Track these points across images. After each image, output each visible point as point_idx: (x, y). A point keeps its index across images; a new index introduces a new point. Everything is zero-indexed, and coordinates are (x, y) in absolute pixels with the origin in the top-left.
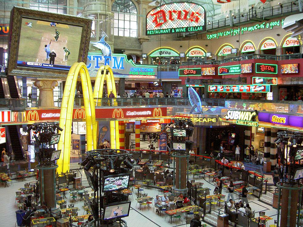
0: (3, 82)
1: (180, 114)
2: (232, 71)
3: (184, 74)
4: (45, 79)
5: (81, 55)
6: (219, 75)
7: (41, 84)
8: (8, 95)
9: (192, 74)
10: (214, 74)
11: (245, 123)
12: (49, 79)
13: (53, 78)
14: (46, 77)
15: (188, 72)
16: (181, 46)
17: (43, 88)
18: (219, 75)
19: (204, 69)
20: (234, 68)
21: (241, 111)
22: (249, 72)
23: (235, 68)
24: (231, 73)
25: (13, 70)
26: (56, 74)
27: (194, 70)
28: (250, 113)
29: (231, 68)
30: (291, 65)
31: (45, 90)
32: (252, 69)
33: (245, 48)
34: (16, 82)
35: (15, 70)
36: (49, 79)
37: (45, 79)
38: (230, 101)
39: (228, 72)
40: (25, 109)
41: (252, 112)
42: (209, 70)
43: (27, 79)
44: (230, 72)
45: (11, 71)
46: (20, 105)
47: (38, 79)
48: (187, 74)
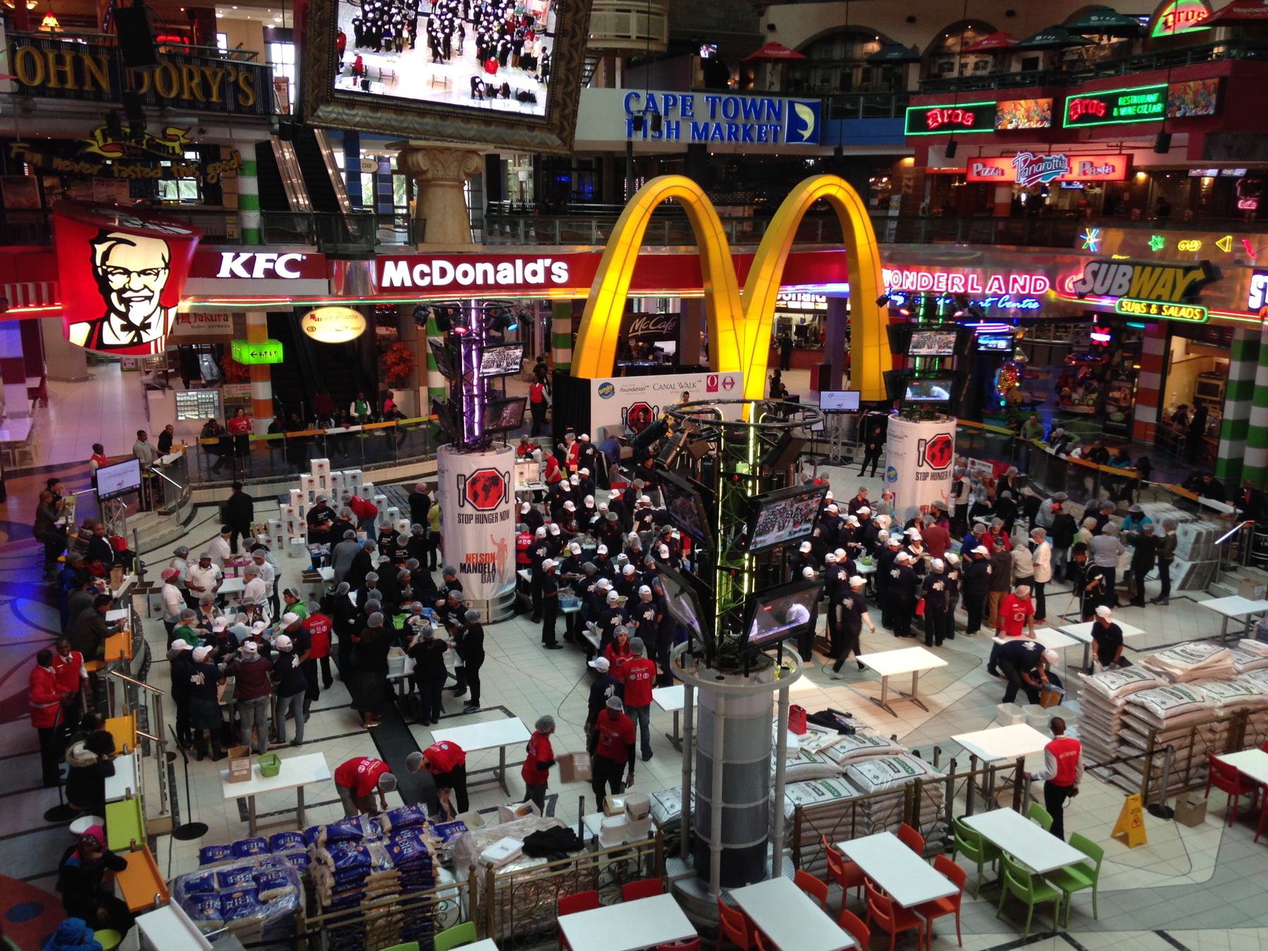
0: (277, 155)
1: (665, 302)
2: (1123, 112)
3: (927, 128)
4: (438, 144)
5: (562, 55)
6: (1065, 126)
7: (420, 160)
8: (303, 200)
9: (961, 126)
10: (1047, 125)
11: (1154, 310)
12: (451, 145)
13: (463, 138)
14: (441, 136)
15: (942, 117)
16: (911, 20)
17: (429, 175)
18: (1065, 126)
19: (1008, 106)
20: (1135, 99)
21: (1144, 266)
22: (1034, 125)
23: (1142, 99)
24: (1120, 117)
25: (322, 107)
26: (475, 126)
27: (966, 110)
28: (1180, 272)
29: (1121, 101)
30: (1031, 103)
31: (442, 186)
32: (1053, 115)
33: (1171, 18)
34: (324, 152)
35: (330, 109)
36: (451, 145)
37: (438, 144)
38: (762, 262)
39: (1108, 115)
40: (372, 251)
41: (1187, 270)
42: (1028, 111)
43: (361, 141)
44: (1115, 113)
45: (315, 110)
46: (348, 238)
47: (413, 143)
48: (941, 127)
